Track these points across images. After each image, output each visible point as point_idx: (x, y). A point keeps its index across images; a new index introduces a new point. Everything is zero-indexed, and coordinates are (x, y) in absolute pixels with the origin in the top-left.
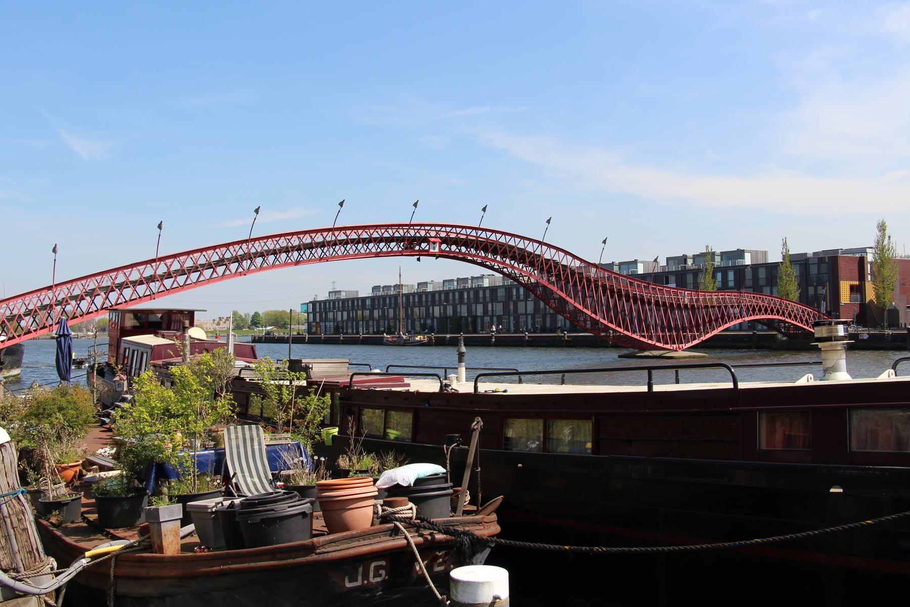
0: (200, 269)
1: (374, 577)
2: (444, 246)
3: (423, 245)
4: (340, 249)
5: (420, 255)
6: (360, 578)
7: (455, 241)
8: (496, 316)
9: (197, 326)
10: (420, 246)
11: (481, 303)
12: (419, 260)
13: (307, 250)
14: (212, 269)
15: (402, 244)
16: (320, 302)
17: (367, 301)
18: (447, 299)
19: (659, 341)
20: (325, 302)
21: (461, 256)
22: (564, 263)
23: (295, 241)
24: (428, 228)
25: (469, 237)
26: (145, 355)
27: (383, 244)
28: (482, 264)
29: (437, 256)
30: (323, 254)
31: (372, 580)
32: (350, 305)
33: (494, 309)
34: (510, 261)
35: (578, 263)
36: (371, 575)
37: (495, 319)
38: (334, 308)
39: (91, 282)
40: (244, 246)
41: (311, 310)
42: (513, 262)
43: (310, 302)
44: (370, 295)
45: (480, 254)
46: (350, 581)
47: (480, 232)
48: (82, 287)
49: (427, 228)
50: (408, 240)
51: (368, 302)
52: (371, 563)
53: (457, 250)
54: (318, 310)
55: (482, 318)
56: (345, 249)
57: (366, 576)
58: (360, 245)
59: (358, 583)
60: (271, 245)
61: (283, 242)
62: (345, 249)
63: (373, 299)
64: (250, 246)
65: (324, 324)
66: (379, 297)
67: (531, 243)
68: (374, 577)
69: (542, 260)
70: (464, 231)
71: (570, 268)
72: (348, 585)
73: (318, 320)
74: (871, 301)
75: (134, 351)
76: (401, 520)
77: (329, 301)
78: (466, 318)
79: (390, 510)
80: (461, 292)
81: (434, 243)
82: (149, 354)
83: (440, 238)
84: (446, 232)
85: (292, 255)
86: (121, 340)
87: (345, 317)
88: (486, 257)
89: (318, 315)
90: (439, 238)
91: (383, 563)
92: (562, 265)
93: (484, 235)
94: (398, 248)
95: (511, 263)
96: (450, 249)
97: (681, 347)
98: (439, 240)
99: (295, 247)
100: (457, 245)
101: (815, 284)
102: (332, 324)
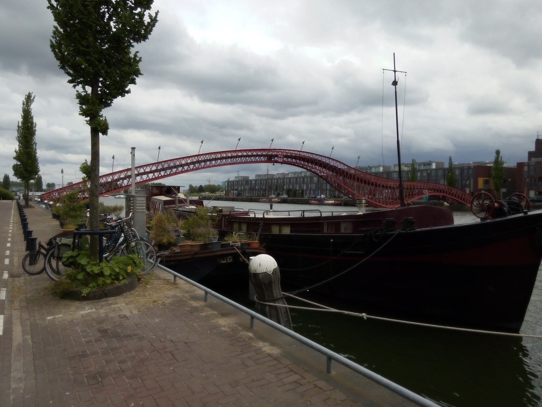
0: (171, 168)
1: (229, 260)
2: (285, 159)
3: (276, 158)
4: (243, 159)
5: (274, 163)
6: (225, 260)
7: (290, 157)
8: (312, 190)
9: (181, 193)
10: (274, 159)
11: (306, 184)
12: (274, 165)
13: (224, 160)
14: (182, 167)
15: (266, 157)
16: (231, 181)
17: (253, 181)
18: (290, 182)
19: (383, 204)
20: (233, 181)
21: (301, 166)
22: (340, 167)
23: (219, 156)
24: (283, 151)
25: (301, 156)
26: (161, 204)
27: (263, 157)
28: (302, 167)
29: (282, 163)
30: (231, 161)
31: (228, 261)
32: (240, 183)
33: (312, 187)
34: (315, 166)
35: (346, 167)
36: (228, 260)
37: (312, 191)
38: (237, 184)
39: (178, 161)
40: (196, 158)
41: (226, 185)
42: (320, 168)
43: (226, 181)
44: (255, 179)
45: (305, 164)
46: (223, 261)
47: (301, 153)
48: (118, 176)
49: (282, 151)
50: (269, 156)
51: (253, 182)
52: (228, 257)
53: (295, 162)
54: (230, 185)
55: (306, 190)
56: (241, 159)
57: (227, 260)
58: (248, 158)
59: (225, 262)
60: (208, 157)
61: (213, 156)
62: (241, 159)
63: (256, 181)
64: (199, 157)
65: (233, 192)
66: (258, 180)
67: (324, 158)
68: (229, 260)
69: (329, 166)
70: (294, 152)
71: (342, 170)
72: (222, 262)
73: (230, 190)
74: (148, 23)
75: (160, 203)
76: (236, 246)
77: (235, 181)
78: (299, 190)
79: (233, 244)
80: (296, 178)
81: (280, 157)
82: (163, 204)
83: (284, 155)
84: (295, 153)
85: (217, 162)
86: (151, 198)
87: (242, 188)
88: (308, 166)
89: (230, 187)
90: (283, 155)
91: (231, 257)
92: (339, 168)
93: (303, 154)
94: (264, 160)
95: (319, 168)
96: (292, 161)
97: (394, 207)
98: (282, 156)
99: (219, 158)
100: (300, 160)
101: (466, 179)
102: (236, 192)
